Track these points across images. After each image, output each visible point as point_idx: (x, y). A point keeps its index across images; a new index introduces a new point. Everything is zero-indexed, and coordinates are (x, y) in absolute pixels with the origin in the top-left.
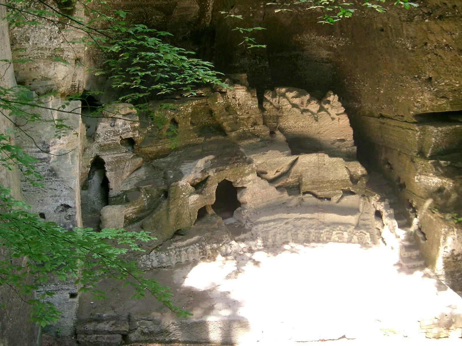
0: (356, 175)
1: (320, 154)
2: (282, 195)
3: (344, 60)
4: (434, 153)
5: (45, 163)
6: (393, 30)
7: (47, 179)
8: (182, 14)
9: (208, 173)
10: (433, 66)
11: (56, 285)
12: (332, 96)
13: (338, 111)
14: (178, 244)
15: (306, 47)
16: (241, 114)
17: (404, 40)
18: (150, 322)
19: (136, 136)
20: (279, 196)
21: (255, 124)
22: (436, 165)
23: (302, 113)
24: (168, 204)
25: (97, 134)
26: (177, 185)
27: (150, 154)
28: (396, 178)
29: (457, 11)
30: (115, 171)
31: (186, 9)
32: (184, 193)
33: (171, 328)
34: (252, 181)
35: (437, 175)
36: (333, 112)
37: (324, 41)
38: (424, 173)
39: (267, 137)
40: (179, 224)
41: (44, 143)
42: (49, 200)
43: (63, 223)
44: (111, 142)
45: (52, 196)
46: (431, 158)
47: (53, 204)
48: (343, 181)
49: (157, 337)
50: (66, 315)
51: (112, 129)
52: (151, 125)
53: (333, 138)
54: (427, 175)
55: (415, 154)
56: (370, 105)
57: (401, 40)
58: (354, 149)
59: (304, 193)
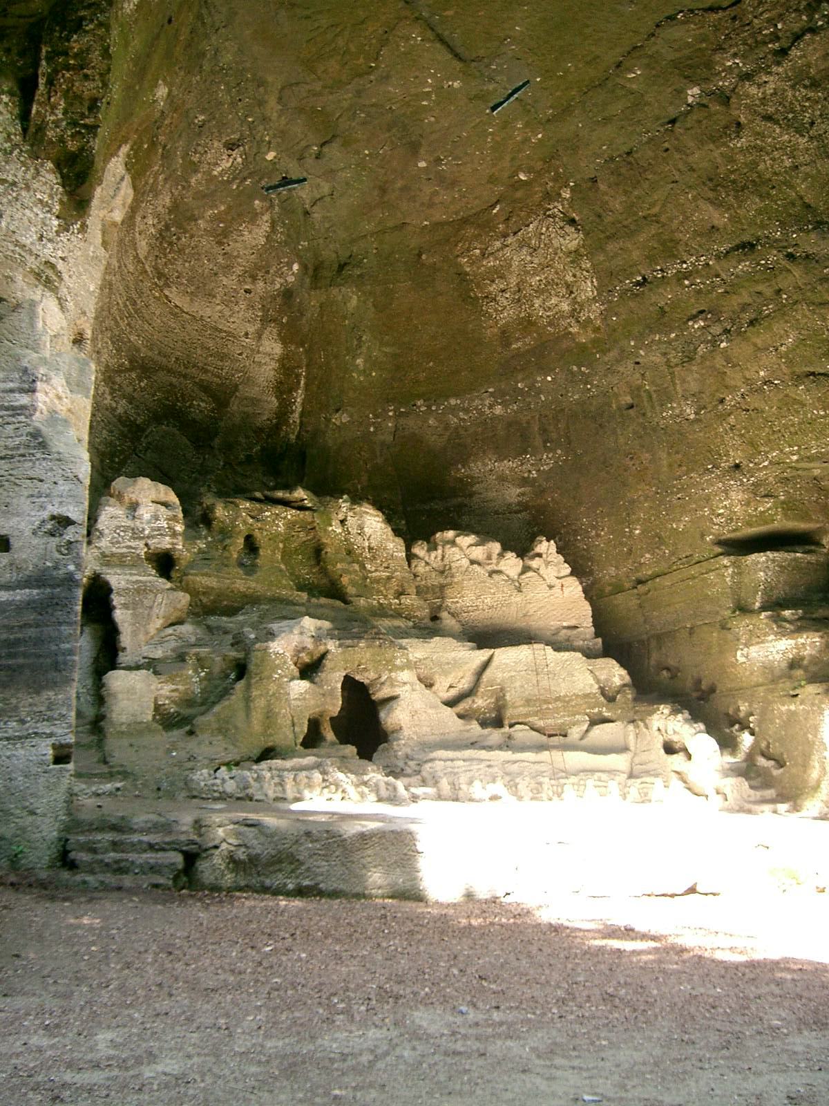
0: (610, 688)
1: (536, 646)
2: (468, 727)
3: (552, 498)
4: (767, 601)
5: (22, 418)
6: (654, 396)
7: (23, 456)
8: (246, 409)
9: (325, 644)
10: (742, 436)
11: (23, 722)
12: (545, 544)
13: (559, 571)
15: (476, 488)
16: (373, 569)
17: (679, 404)
18: (252, 829)
20: (462, 728)
21: (400, 594)
22: (777, 619)
23: (490, 576)
24: (248, 687)
25: (97, 530)
27: (204, 593)
28: (689, 684)
29: (785, 296)
30: (134, 609)
31: (255, 402)
33: (301, 848)
35: (783, 634)
36: (550, 573)
37: (512, 469)
38: (755, 640)
40: (271, 735)
41: (25, 371)
42: (24, 504)
43: (52, 560)
44: (125, 550)
45: (32, 496)
46: (764, 608)
47: (33, 513)
48: (587, 696)
49: (267, 877)
50: (41, 805)
52: (206, 538)
53: (554, 624)
54: (762, 642)
55: (728, 613)
56: (612, 571)
57: (672, 408)
58: (596, 644)
59: (511, 726)
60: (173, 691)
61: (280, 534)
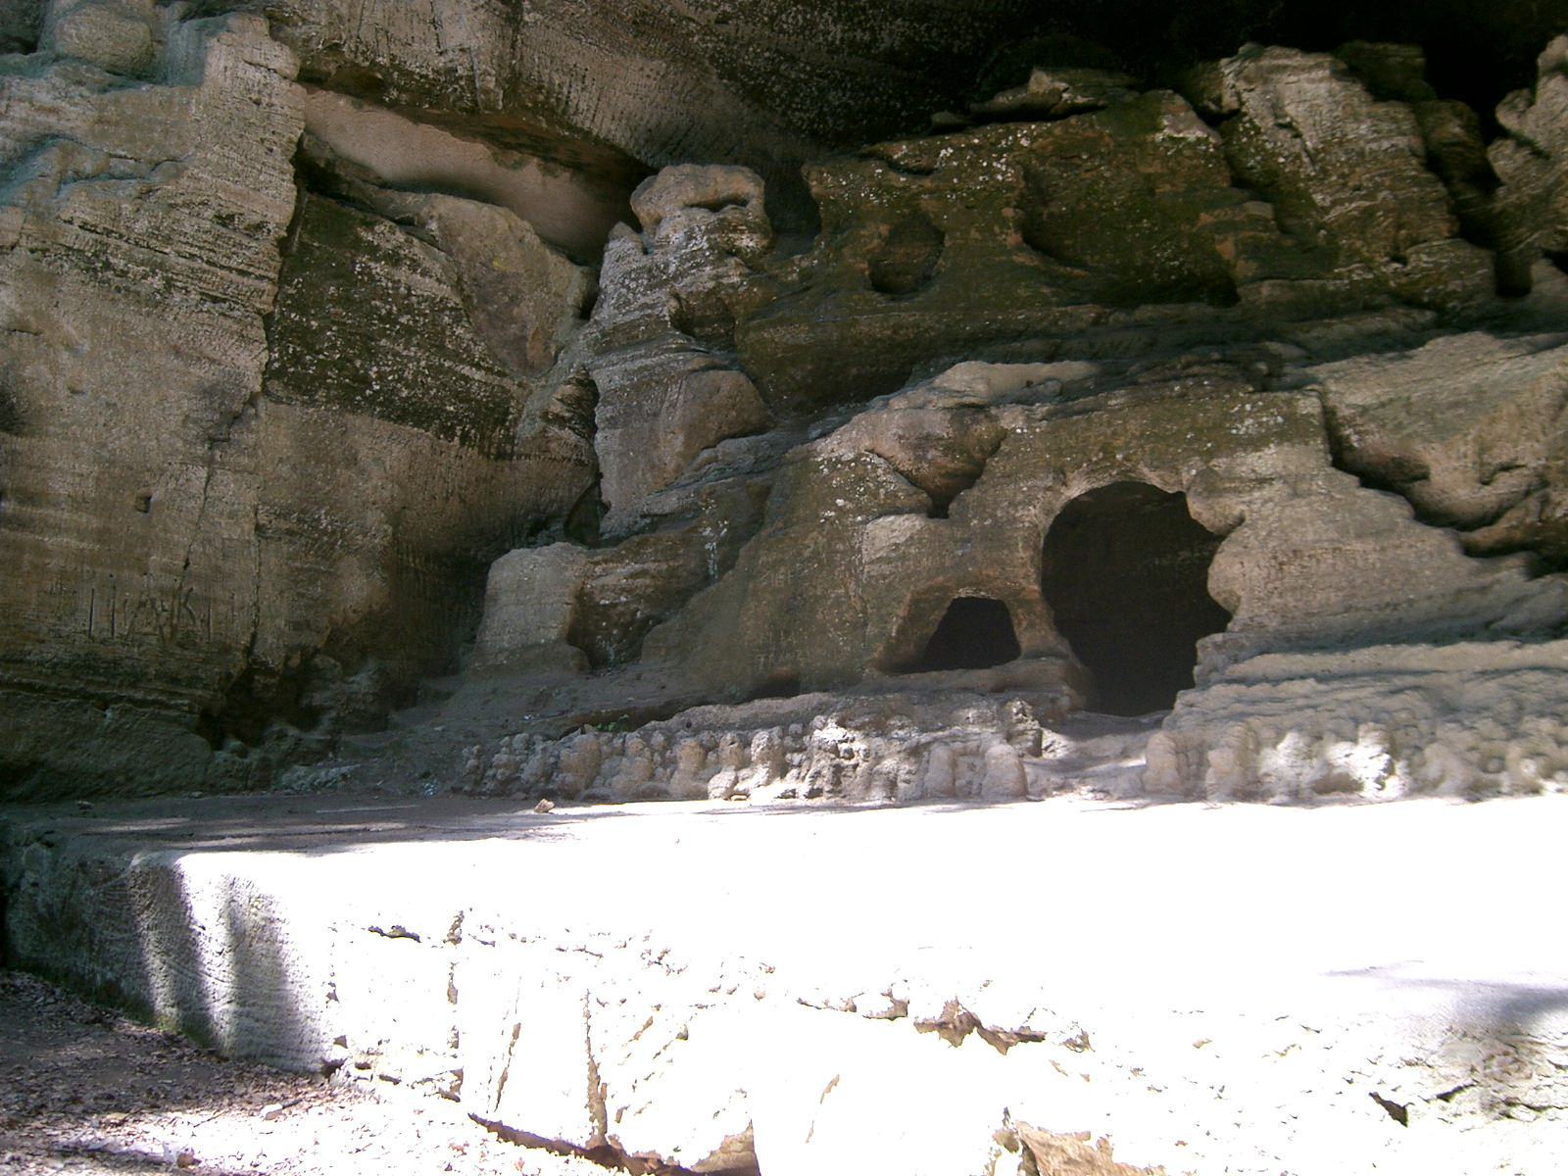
2: (1488, 579)
14: (704, 713)
19: (725, 281)
26: (805, 459)
30: (625, 425)
32: (840, 502)
34: (1278, 485)
39: (1479, 299)
51: (645, 261)
60: (633, 576)
61: (1000, 187)
